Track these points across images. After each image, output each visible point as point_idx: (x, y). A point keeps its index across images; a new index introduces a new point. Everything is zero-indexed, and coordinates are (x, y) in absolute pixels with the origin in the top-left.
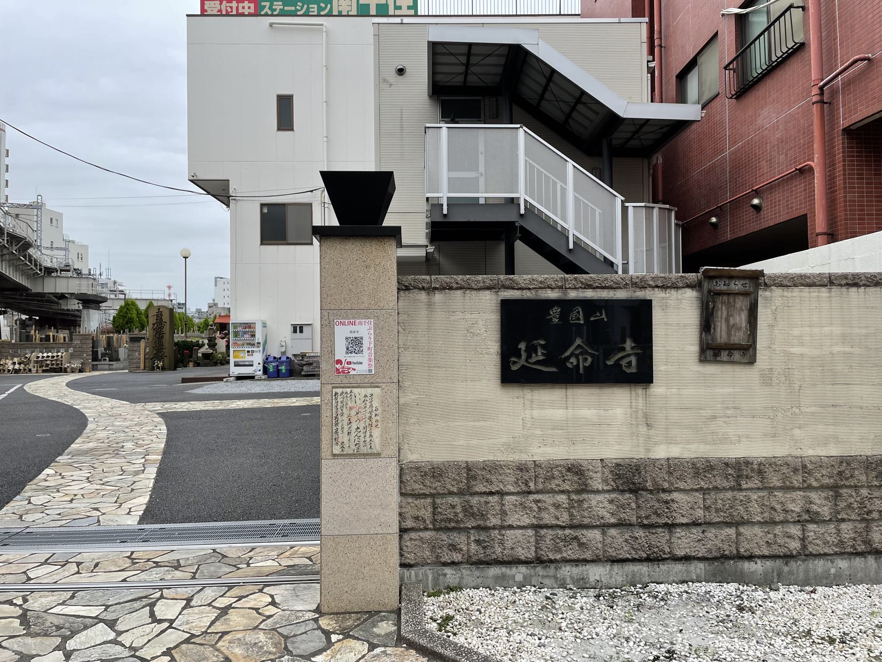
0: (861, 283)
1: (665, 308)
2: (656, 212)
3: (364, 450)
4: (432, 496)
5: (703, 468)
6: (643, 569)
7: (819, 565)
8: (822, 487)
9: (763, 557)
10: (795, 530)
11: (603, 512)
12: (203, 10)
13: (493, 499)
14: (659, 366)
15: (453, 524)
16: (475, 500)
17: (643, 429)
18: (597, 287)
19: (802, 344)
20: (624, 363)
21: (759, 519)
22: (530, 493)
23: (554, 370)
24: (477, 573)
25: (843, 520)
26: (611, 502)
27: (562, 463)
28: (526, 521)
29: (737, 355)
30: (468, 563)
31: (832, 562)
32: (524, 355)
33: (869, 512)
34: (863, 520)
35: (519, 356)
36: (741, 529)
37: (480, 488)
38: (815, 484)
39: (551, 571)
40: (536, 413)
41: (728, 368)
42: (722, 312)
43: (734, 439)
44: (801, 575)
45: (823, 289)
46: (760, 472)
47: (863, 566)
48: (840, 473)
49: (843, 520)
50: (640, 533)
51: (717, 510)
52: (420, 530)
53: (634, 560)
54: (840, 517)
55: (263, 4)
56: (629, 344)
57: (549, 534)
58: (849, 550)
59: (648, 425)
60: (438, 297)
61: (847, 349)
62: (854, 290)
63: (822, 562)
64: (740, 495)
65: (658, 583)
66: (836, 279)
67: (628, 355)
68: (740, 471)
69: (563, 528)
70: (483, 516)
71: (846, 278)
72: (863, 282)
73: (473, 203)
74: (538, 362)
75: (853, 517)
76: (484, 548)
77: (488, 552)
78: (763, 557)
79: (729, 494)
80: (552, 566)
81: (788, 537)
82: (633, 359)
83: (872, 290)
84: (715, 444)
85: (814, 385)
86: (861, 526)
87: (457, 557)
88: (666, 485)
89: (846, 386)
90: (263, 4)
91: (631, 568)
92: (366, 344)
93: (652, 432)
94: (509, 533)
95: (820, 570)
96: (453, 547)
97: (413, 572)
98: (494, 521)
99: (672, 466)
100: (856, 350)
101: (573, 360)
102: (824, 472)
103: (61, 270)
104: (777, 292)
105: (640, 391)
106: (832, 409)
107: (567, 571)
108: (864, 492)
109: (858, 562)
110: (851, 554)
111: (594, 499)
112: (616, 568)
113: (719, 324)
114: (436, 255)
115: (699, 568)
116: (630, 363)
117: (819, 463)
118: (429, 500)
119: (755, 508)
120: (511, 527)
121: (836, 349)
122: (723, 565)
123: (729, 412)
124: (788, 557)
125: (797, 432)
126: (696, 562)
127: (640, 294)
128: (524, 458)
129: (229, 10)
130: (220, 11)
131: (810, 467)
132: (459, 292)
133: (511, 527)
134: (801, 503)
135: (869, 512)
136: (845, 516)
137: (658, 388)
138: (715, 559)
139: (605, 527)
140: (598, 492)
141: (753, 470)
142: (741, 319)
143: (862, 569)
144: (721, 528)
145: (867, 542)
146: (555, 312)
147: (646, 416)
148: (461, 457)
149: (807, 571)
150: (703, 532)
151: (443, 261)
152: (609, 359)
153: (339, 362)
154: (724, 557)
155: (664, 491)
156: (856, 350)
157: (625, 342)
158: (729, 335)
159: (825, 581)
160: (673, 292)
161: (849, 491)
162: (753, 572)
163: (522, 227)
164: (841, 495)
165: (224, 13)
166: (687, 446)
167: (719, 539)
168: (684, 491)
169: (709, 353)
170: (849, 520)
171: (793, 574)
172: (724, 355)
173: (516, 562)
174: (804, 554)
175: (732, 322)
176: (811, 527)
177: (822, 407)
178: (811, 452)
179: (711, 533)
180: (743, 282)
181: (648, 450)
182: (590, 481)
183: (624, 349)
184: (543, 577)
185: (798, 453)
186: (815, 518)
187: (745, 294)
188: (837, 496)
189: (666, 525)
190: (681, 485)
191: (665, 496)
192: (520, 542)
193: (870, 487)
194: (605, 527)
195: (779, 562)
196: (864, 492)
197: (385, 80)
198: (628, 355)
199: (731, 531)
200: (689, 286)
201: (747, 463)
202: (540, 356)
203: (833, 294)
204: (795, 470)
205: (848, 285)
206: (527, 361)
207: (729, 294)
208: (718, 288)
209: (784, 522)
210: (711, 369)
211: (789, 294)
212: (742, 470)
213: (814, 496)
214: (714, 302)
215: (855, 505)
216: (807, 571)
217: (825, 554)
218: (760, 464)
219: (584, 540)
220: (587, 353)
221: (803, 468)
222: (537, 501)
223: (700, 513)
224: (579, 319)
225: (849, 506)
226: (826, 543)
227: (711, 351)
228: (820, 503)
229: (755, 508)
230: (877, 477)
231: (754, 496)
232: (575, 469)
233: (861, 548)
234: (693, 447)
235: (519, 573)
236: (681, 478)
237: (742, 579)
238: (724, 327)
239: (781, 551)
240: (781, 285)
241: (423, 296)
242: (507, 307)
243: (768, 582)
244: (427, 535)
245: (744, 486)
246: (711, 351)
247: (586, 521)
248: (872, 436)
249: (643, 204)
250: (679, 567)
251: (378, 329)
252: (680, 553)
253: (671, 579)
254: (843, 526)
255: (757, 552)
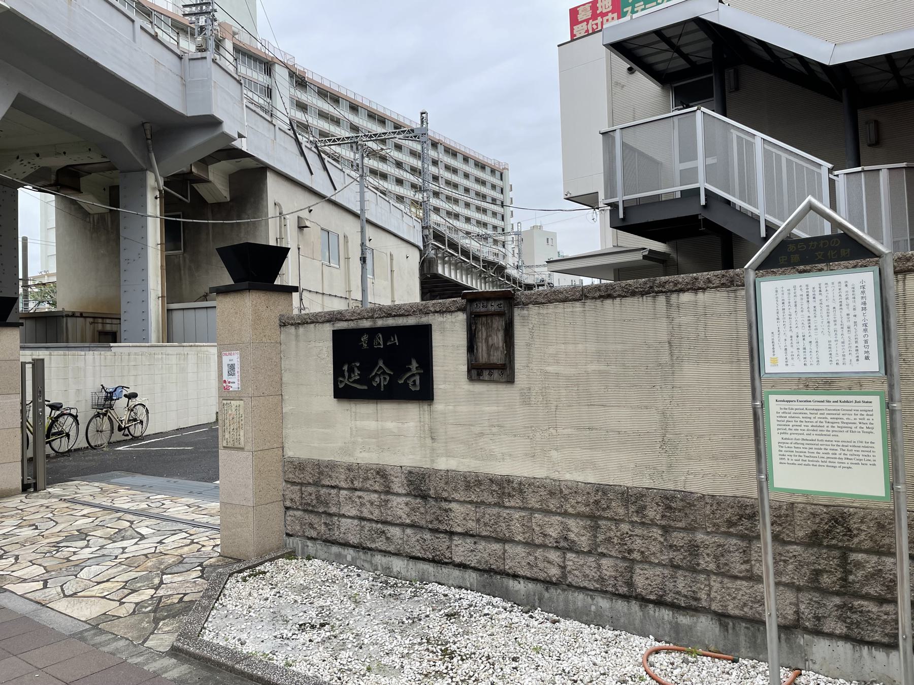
0: (615, 294)
1: (443, 330)
2: (884, 176)
3: (237, 445)
4: (301, 484)
5: (472, 482)
6: (430, 568)
7: (580, 599)
8: (578, 515)
9: (526, 578)
10: (554, 556)
11: (400, 513)
12: (572, 35)
13: (334, 492)
14: (439, 386)
15: (311, 508)
16: (323, 491)
17: (428, 441)
18: (395, 316)
19: (558, 363)
20: (410, 382)
21: (521, 539)
22: (356, 490)
23: (366, 388)
24: (325, 549)
25: (603, 555)
26: (407, 504)
27: (374, 467)
28: (354, 512)
29: (496, 375)
30: (321, 540)
31: (593, 599)
32: (346, 374)
33: (630, 551)
34: (624, 559)
35: (344, 376)
36: (507, 547)
37: (326, 482)
38: (570, 510)
39: (368, 557)
40: (359, 423)
41: (492, 387)
42: (482, 334)
43: (499, 456)
44: (561, 606)
45: (578, 304)
46: (521, 492)
47: (625, 610)
48: (597, 502)
49: (603, 555)
50: (428, 536)
51: (485, 524)
52: (294, 509)
53: (424, 559)
54: (599, 550)
55: (625, 10)
56: (414, 365)
57: (367, 525)
58: (610, 589)
59: (432, 438)
60: (301, 329)
61: (603, 368)
62: (608, 302)
63: (581, 596)
64: (504, 513)
65: (439, 584)
66: (589, 292)
67: (413, 375)
68: (504, 488)
69: (377, 522)
70: (327, 504)
71: (599, 290)
72: (617, 293)
73: (655, 201)
74: (355, 382)
75: (613, 553)
76: (329, 530)
77: (331, 533)
78: (526, 578)
79: (495, 510)
80: (369, 553)
81: (549, 562)
82: (417, 378)
83: (629, 301)
84: (483, 460)
85: (569, 406)
86: (622, 565)
87: (314, 534)
88: (445, 495)
89: (602, 408)
90: (625, 10)
91: (422, 566)
92: (236, 370)
93: (435, 445)
94: (343, 520)
95: (580, 604)
96: (311, 526)
97: (291, 539)
98: (333, 510)
99: (449, 477)
100: (613, 369)
101: (377, 379)
102: (580, 500)
103: (539, 286)
104: (534, 310)
105: (426, 407)
106: (588, 432)
107: (379, 559)
108: (625, 527)
109: (620, 605)
110: (614, 594)
111: (396, 501)
112: (411, 564)
113: (480, 344)
114: (674, 255)
115: (472, 577)
116: (414, 381)
117: (575, 489)
118: (298, 487)
119: (516, 527)
120: (344, 516)
121: (592, 367)
122: (493, 578)
123: (495, 430)
124: (548, 583)
125: (554, 453)
126: (470, 571)
127: (425, 320)
128: (351, 460)
129: (595, 27)
130: (587, 31)
131: (566, 492)
132: (312, 325)
133: (344, 516)
134: (559, 529)
135: (630, 551)
136: (605, 551)
137: (439, 405)
138: (484, 571)
139: (403, 525)
140: (398, 495)
141: (514, 489)
142: (498, 339)
143: (625, 614)
144: (489, 542)
145: (630, 584)
146: (365, 338)
147: (431, 430)
148: (316, 456)
149: (566, 601)
150: (475, 543)
151: (681, 260)
152: (401, 379)
153: (225, 382)
154: (490, 571)
155: (446, 500)
156: (613, 369)
157: (410, 363)
158: (489, 355)
159: (585, 618)
160: (448, 316)
161: (609, 523)
162: (517, 591)
163: (705, 220)
164: (599, 527)
165: (590, 32)
166: (463, 460)
167: (486, 552)
168: (457, 501)
169: (474, 372)
170: (611, 556)
171: (553, 602)
172: (486, 373)
173: (346, 545)
174: (560, 583)
175: (490, 343)
176: (569, 555)
177: (579, 429)
178: (568, 477)
179: (482, 545)
180: (498, 302)
181: (433, 461)
182: (391, 484)
183: (410, 370)
184: (364, 560)
185: (555, 476)
186: (572, 548)
187: (500, 314)
188: (596, 528)
189: (446, 532)
190: (456, 496)
191: (444, 505)
192: (348, 529)
193: (632, 523)
194: (403, 525)
195: (539, 587)
196: (625, 527)
197: (617, 84)
198: (413, 375)
199: (496, 546)
200: (459, 310)
201: (508, 480)
202: (356, 375)
203: (587, 309)
204: (552, 494)
205: (603, 297)
206: (350, 377)
207: (486, 315)
208: (478, 310)
209: (544, 546)
210: (479, 388)
211: (545, 311)
212: (504, 488)
213: (571, 523)
214: (476, 324)
215: (615, 541)
216: (566, 601)
217: (585, 588)
218: (520, 484)
219: (389, 535)
220: (384, 373)
221: (555, 490)
222: (360, 497)
223: (471, 525)
224: (379, 344)
225: (609, 540)
226: (586, 576)
227: (477, 371)
228: (578, 531)
229: (516, 527)
230: (637, 512)
231: (517, 515)
232: (382, 473)
233: (623, 590)
234: (466, 461)
235: (350, 553)
236: (455, 489)
237: (506, 595)
238: (484, 348)
239: (542, 576)
240: (536, 303)
241: (292, 330)
242: (336, 333)
243: (528, 606)
244: (298, 513)
245: (507, 504)
246: (477, 371)
247: (389, 519)
248: (632, 465)
249: (904, 165)
250: (456, 573)
251: (242, 358)
252: (457, 560)
253: (450, 582)
254: (604, 562)
255: (521, 573)
